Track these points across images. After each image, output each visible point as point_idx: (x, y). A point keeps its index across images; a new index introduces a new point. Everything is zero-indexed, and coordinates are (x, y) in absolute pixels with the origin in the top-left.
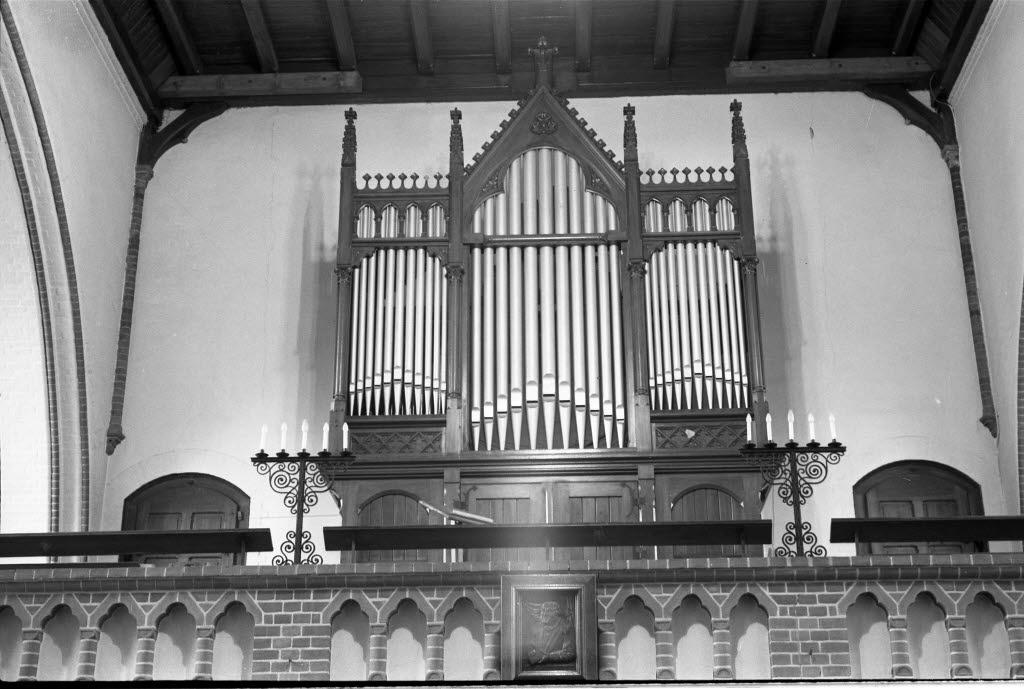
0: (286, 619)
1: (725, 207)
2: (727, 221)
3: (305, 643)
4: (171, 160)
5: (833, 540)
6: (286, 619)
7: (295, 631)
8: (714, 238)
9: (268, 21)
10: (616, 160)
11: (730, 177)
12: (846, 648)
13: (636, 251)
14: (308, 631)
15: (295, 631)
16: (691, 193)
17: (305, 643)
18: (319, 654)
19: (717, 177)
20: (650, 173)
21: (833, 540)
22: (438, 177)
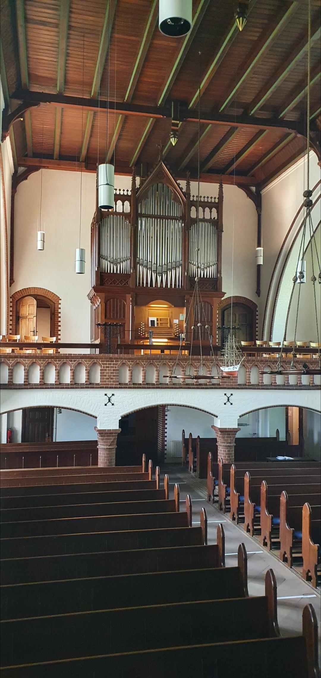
0: (109, 367)
1: (214, 210)
2: (214, 215)
3: (113, 373)
4: (23, 185)
5: (215, 440)
6: (109, 367)
7: (111, 370)
8: (211, 221)
9: (32, 128)
10: (183, 191)
11: (217, 201)
12: (265, 58)
13: (189, 223)
14: (114, 370)
15: (111, 370)
16: (205, 205)
17: (113, 373)
18: (117, 376)
19: (213, 200)
20: (193, 196)
21: (215, 440)
22: (128, 191)
